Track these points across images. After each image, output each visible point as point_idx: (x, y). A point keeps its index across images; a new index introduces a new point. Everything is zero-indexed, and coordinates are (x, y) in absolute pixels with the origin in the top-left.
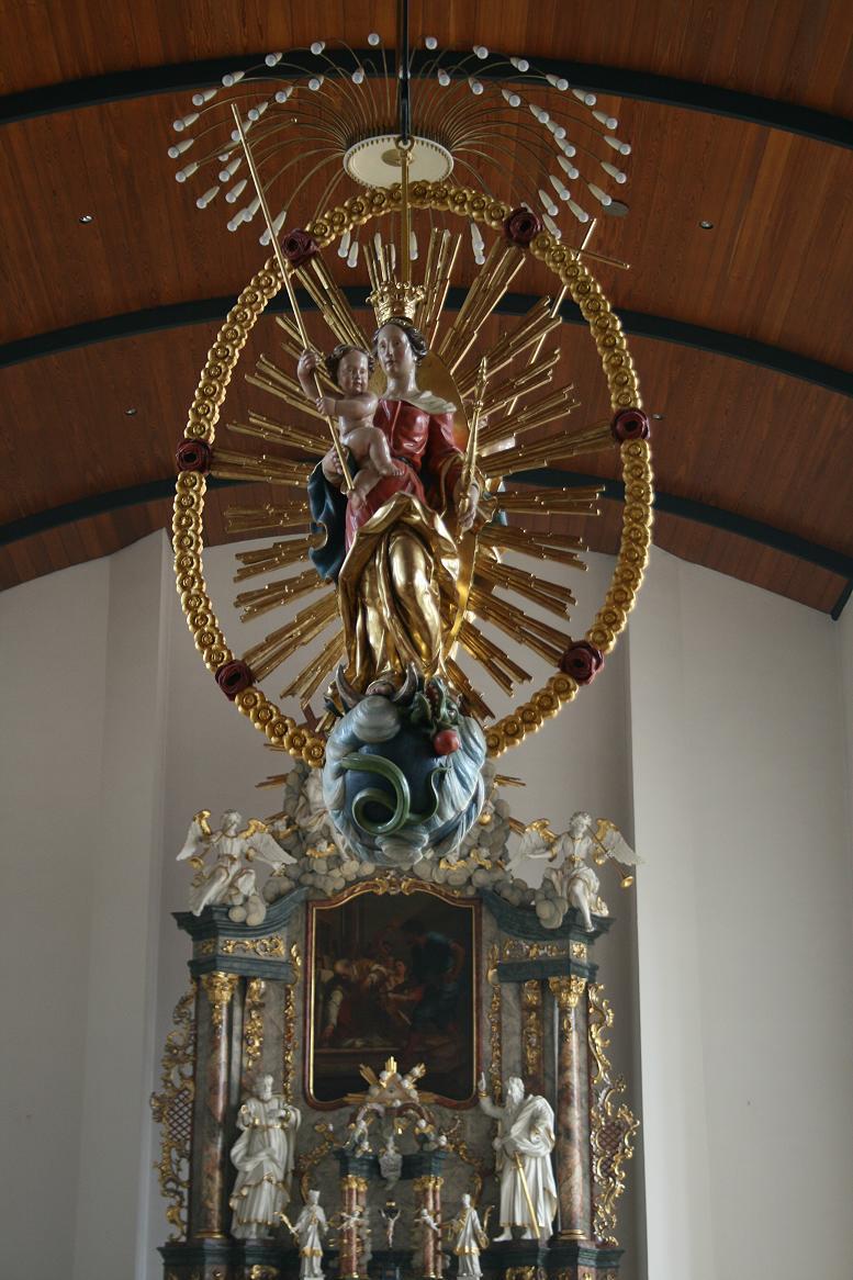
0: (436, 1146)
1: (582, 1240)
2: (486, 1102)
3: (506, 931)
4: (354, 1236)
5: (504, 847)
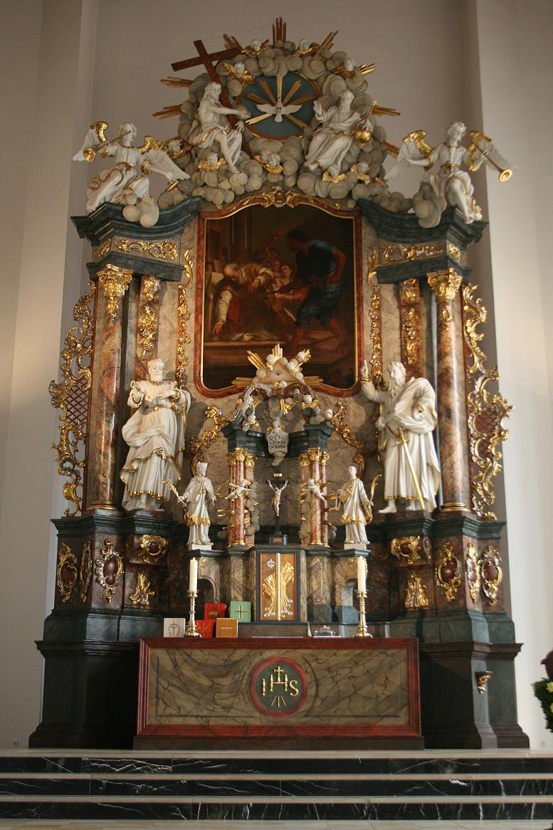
0: (323, 419)
1: (465, 512)
2: (369, 388)
3: (384, 238)
4: (242, 507)
5: (381, 167)
